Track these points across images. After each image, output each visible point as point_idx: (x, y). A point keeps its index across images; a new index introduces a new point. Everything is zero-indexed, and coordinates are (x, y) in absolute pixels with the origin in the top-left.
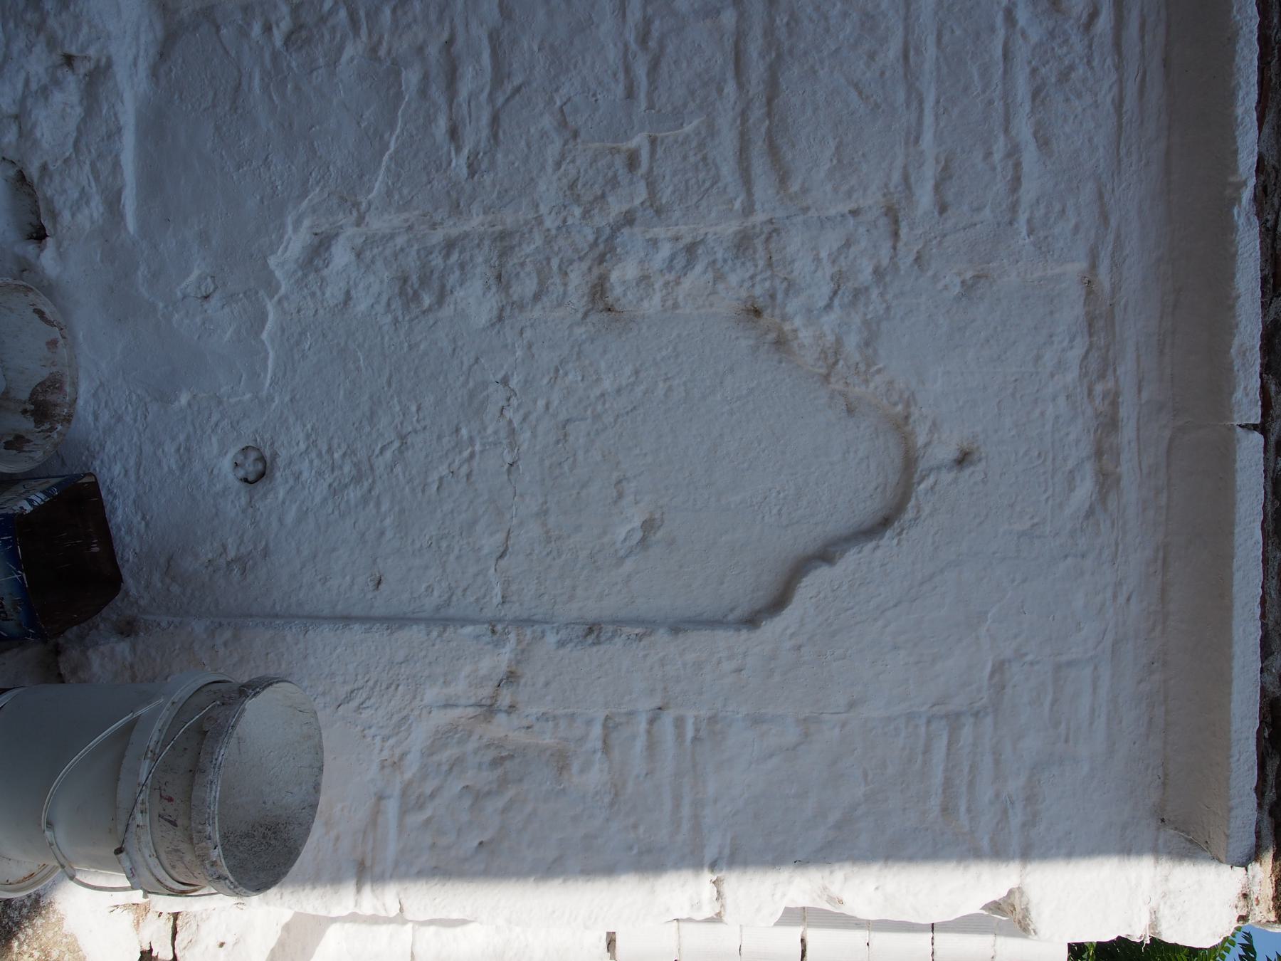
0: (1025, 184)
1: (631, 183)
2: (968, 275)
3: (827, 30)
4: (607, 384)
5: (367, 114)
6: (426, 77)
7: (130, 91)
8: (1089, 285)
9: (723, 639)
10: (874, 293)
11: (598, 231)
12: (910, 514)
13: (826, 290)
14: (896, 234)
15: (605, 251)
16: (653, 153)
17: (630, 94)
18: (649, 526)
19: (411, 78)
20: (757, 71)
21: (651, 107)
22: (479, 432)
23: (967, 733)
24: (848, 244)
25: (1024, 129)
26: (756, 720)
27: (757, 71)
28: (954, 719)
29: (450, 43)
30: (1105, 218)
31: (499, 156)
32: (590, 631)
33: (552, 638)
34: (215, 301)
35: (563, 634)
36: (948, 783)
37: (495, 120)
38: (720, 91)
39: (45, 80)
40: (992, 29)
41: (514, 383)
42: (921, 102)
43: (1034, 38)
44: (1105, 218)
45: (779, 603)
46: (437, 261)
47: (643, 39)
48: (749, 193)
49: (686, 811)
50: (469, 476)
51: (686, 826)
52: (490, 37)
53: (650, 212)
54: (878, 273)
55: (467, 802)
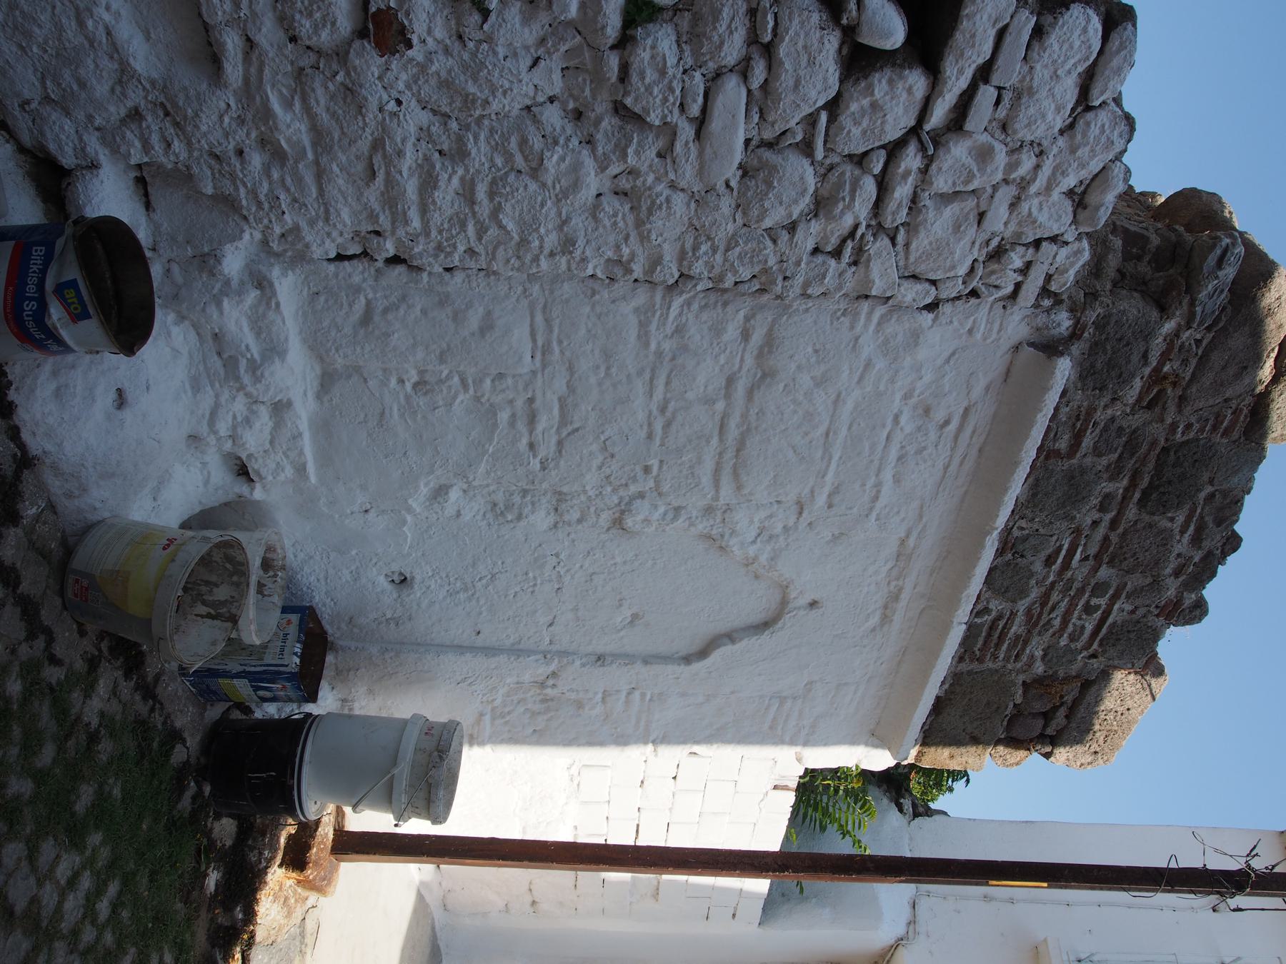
0: (880, 499)
1: (645, 480)
3: (781, 420)
4: (618, 560)
5: (473, 433)
6: (513, 415)
7: (304, 411)
8: (903, 542)
9: (671, 669)
10: (781, 538)
11: (621, 499)
12: (780, 624)
13: (754, 534)
14: (800, 513)
16: (660, 467)
17: (650, 436)
18: (635, 617)
19: (504, 416)
20: (733, 432)
21: (662, 445)
24: (771, 516)
25: (887, 475)
26: (683, 695)
27: (733, 432)
28: (783, 700)
29: (531, 400)
30: (921, 517)
31: (562, 462)
32: (599, 659)
33: (578, 663)
34: (372, 514)
35: (584, 660)
36: (774, 719)
37: (560, 443)
38: (708, 442)
39: (245, 413)
40: (884, 426)
41: (562, 556)
42: (830, 459)
43: (908, 429)
44: (921, 517)
45: (703, 653)
46: (517, 499)
47: (663, 410)
48: (717, 491)
49: (642, 723)
50: (533, 592)
52: (560, 399)
53: (655, 494)
54: (786, 529)
55: (528, 715)
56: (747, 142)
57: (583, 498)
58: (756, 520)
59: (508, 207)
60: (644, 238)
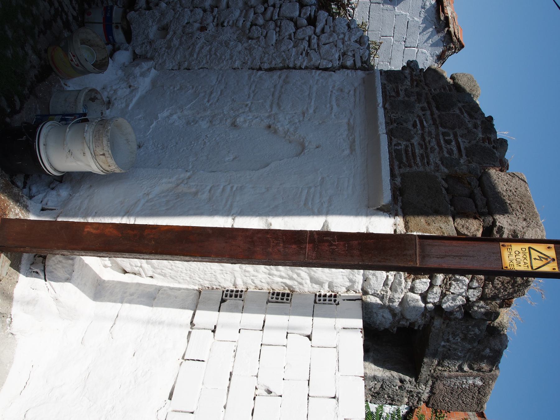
2: (320, 122)
4: (231, 137)
8: (349, 124)
15: (236, 117)
22: (191, 275)
23: (312, 190)
30: (352, 115)
36: (306, 199)
44: (352, 115)
49: (229, 203)
51: (228, 206)
54: (299, 121)
56: (276, 40)
57: (222, 115)
58: (287, 118)
59: (219, 51)
60: (251, 55)
